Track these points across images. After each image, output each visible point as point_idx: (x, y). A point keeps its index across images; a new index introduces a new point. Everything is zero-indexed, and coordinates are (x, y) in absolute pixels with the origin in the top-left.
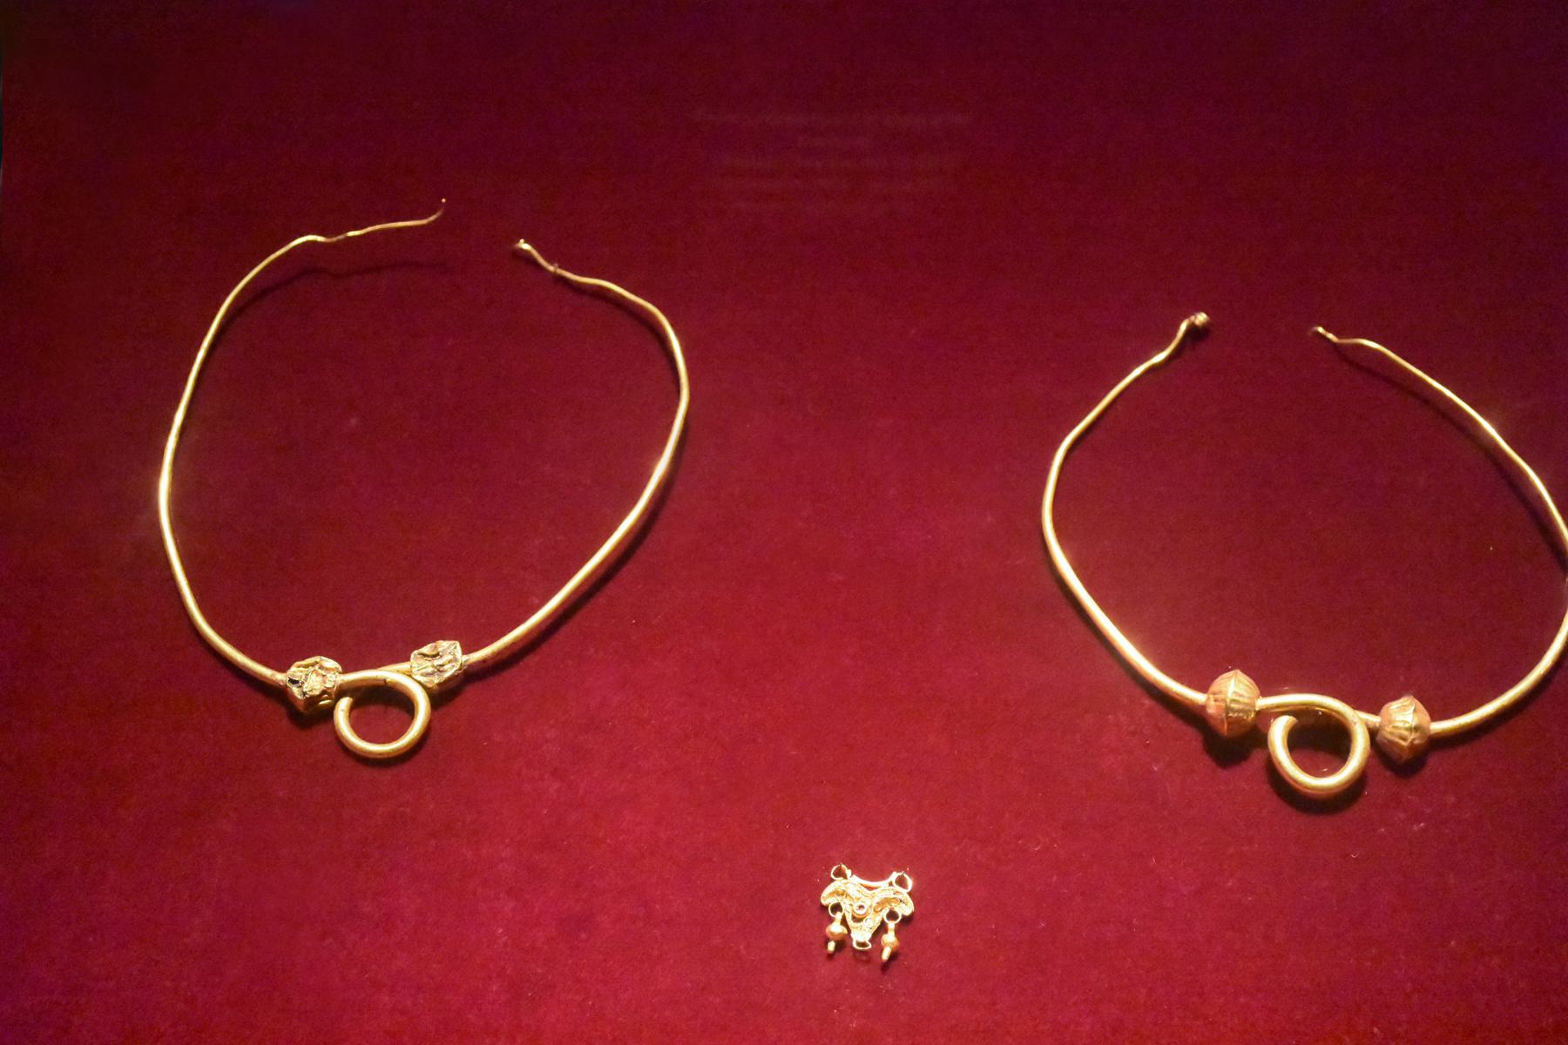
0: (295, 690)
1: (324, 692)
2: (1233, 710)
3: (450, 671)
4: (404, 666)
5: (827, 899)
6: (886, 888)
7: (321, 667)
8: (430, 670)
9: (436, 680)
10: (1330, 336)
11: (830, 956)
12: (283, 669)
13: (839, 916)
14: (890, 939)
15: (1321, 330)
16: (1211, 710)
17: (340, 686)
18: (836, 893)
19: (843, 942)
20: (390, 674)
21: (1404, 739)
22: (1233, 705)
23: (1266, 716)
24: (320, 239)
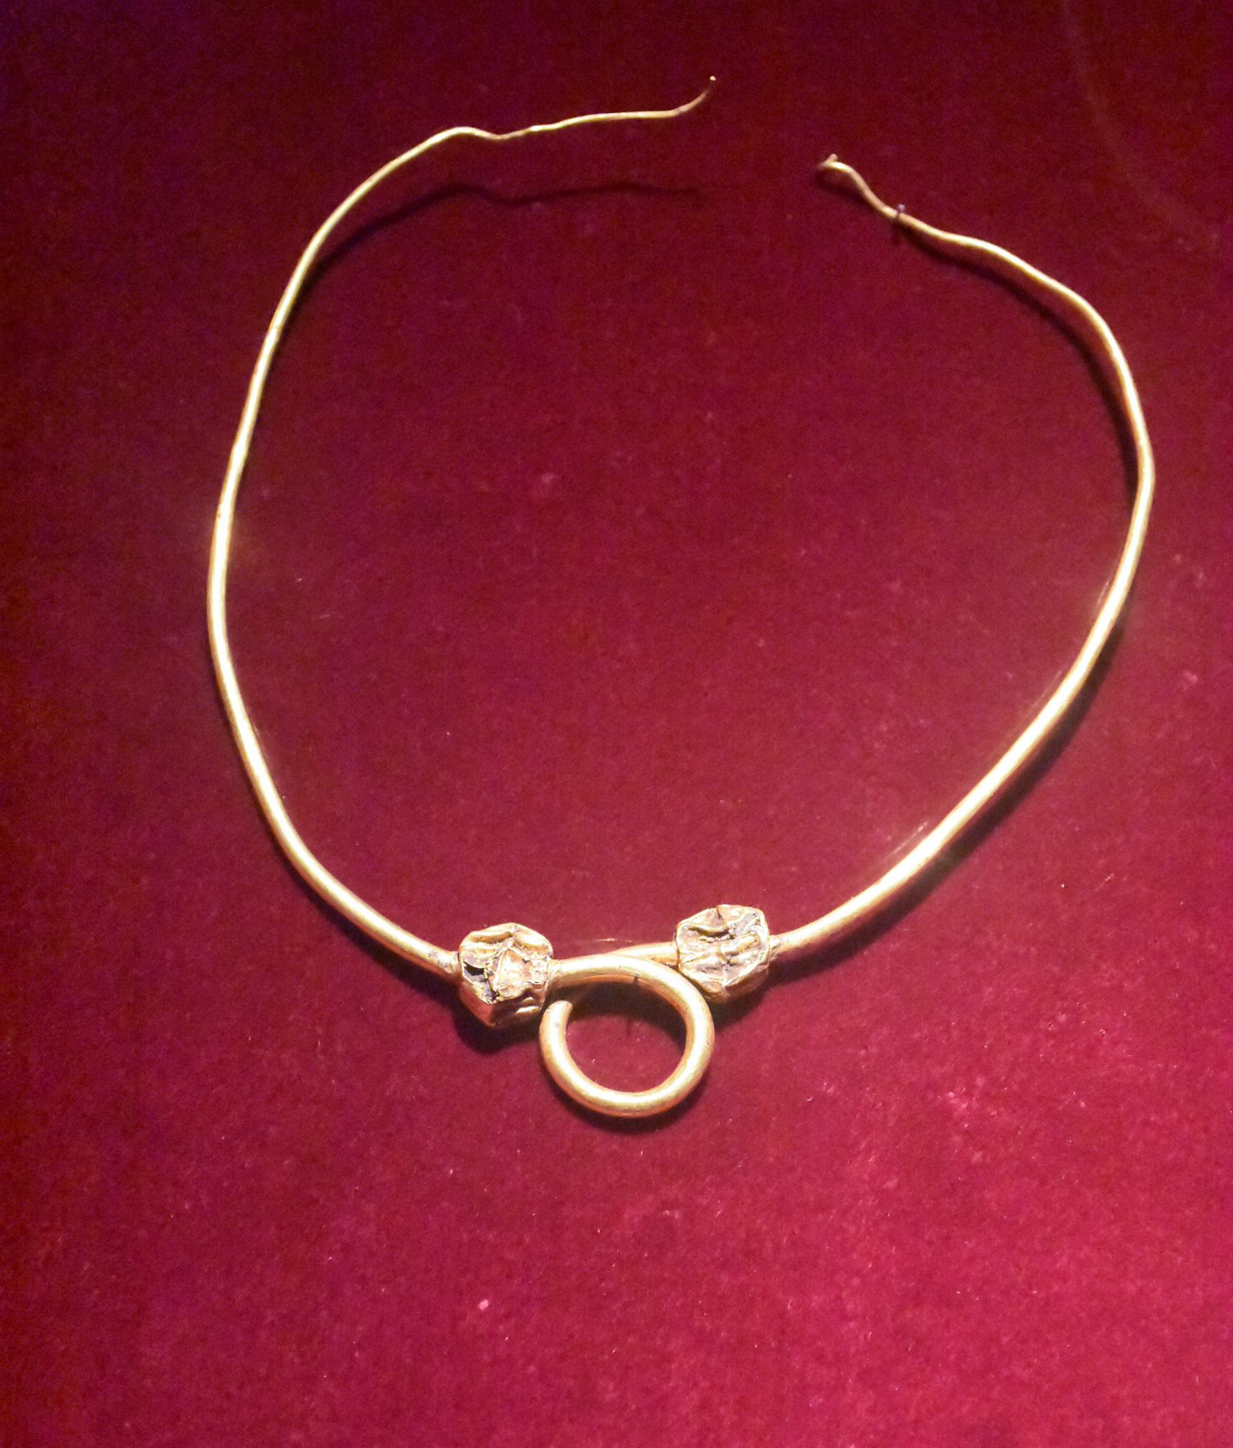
0: (479, 989)
1: (527, 993)
3: (749, 965)
4: (664, 950)
7: (517, 944)
8: (713, 960)
12: (451, 942)
20: (635, 961)
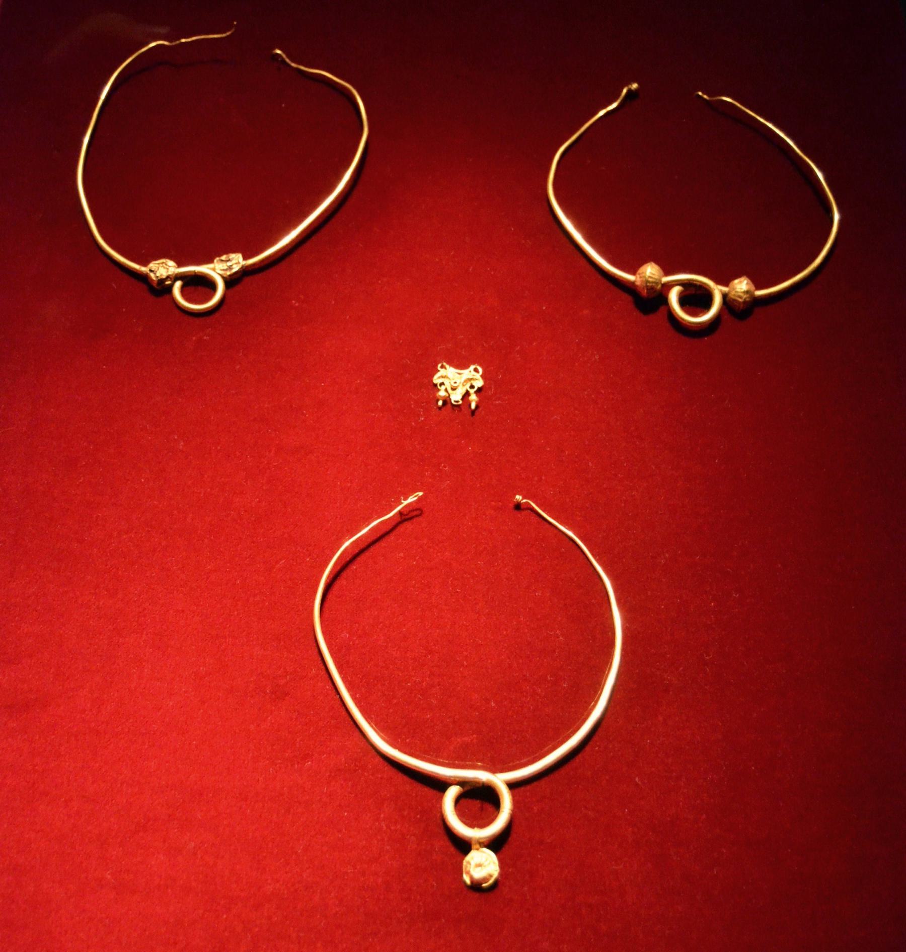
0: (152, 275)
2: (649, 282)
3: (236, 268)
4: (211, 266)
5: (436, 380)
6: (469, 373)
8: (225, 267)
9: (229, 273)
10: (705, 97)
11: (440, 408)
13: (443, 388)
14: (473, 398)
15: (700, 93)
16: (638, 283)
17: (177, 275)
18: (442, 377)
19: (447, 401)
21: (741, 297)
22: (650, 280)
23: (668, 286)
24: (166, 43)
